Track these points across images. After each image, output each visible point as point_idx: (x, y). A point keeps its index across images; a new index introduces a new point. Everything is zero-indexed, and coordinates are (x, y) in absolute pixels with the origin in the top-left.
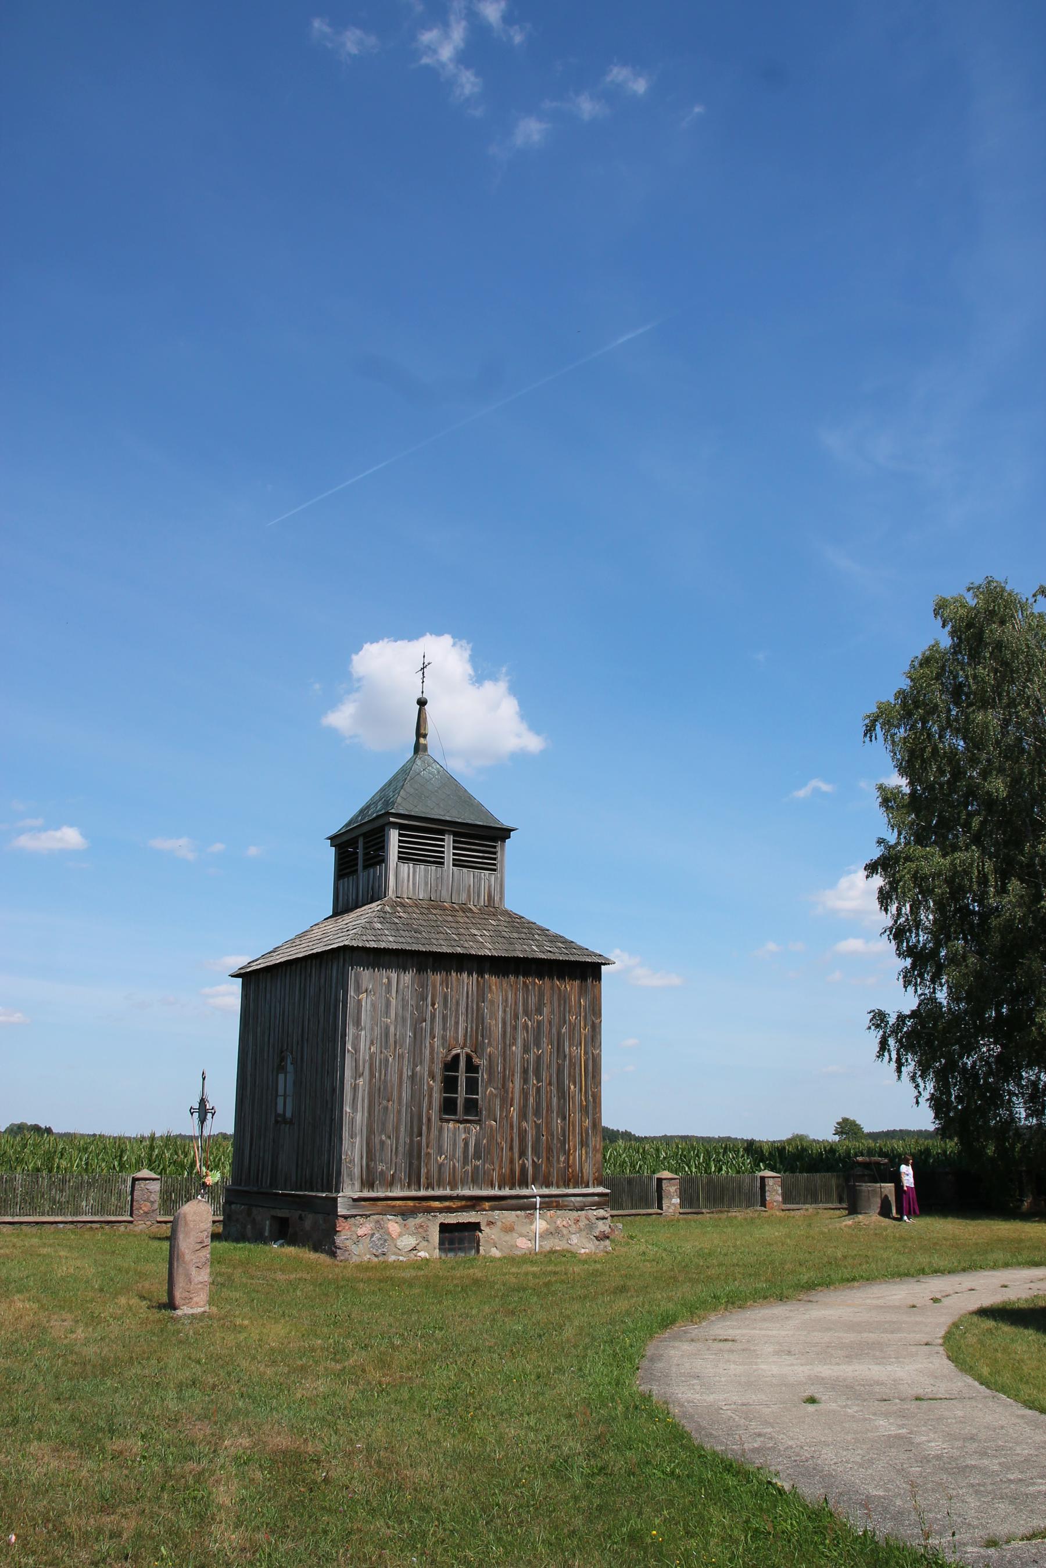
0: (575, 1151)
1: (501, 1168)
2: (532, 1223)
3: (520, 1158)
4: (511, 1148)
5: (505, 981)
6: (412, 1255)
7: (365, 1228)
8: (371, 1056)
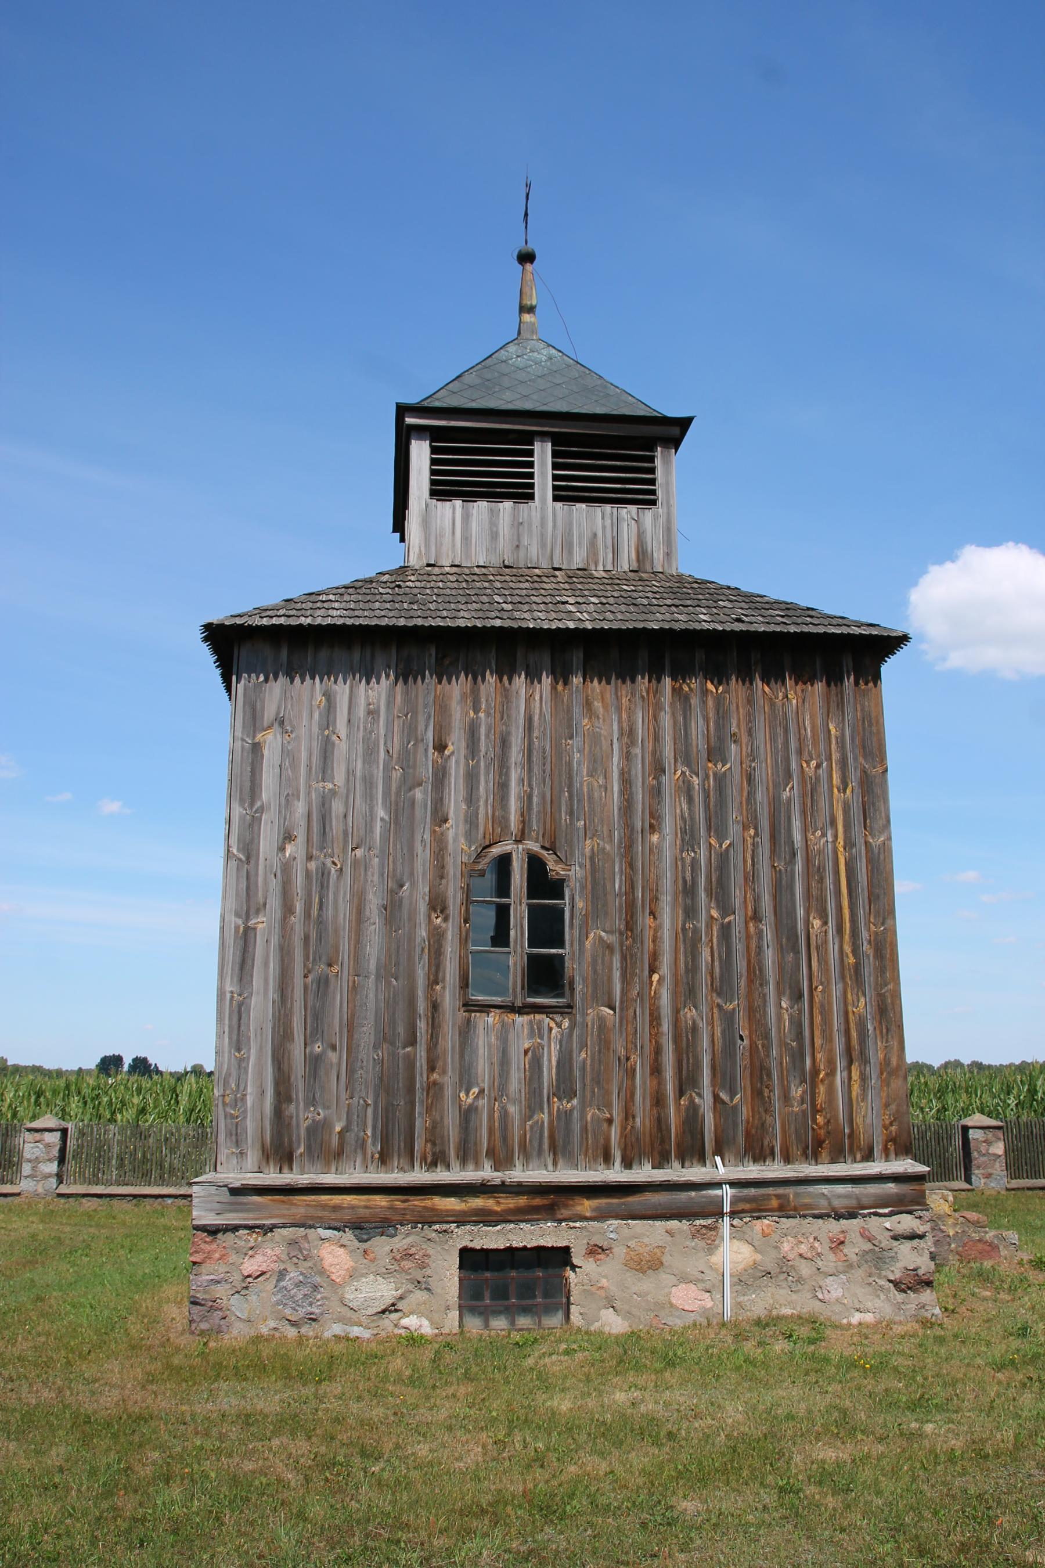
0: (831, 1073)
1: (628, 1115)
2: (712, 1248)
3: (681, 1093)
4: (656, 1070)
5: (625, 689)
6: (387, 1322)
7: (265, 1256)
8: (286, 868)
